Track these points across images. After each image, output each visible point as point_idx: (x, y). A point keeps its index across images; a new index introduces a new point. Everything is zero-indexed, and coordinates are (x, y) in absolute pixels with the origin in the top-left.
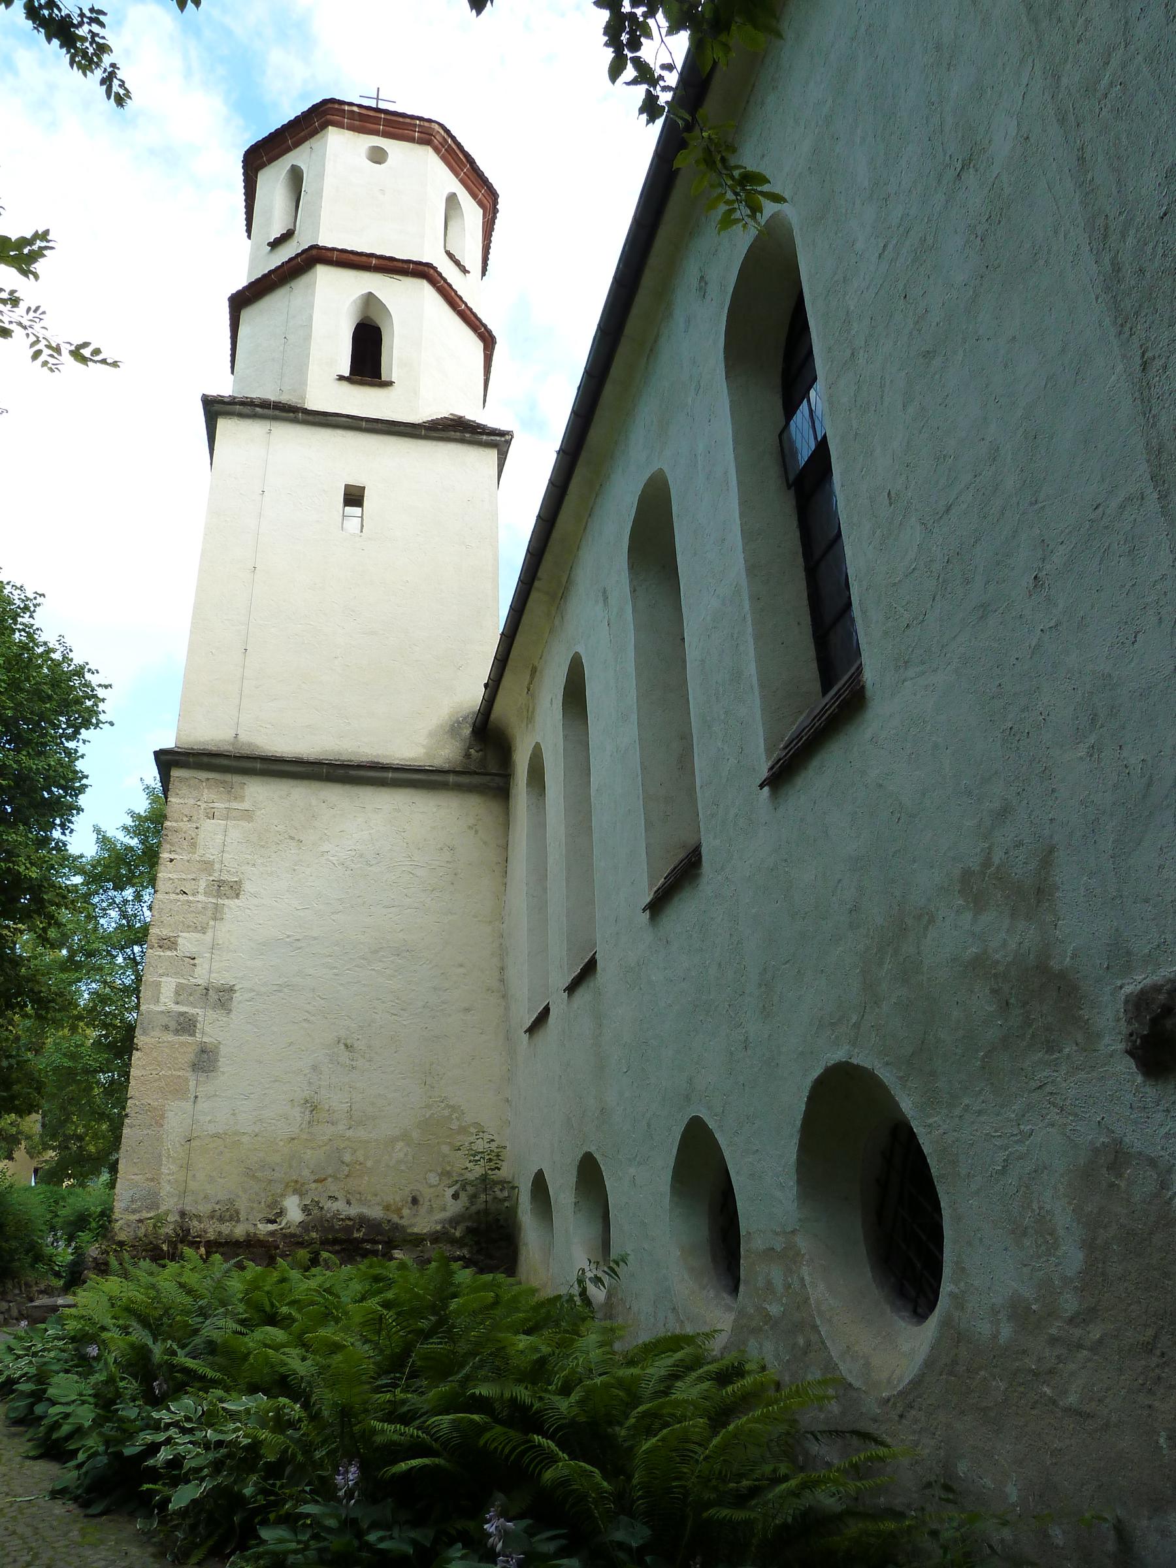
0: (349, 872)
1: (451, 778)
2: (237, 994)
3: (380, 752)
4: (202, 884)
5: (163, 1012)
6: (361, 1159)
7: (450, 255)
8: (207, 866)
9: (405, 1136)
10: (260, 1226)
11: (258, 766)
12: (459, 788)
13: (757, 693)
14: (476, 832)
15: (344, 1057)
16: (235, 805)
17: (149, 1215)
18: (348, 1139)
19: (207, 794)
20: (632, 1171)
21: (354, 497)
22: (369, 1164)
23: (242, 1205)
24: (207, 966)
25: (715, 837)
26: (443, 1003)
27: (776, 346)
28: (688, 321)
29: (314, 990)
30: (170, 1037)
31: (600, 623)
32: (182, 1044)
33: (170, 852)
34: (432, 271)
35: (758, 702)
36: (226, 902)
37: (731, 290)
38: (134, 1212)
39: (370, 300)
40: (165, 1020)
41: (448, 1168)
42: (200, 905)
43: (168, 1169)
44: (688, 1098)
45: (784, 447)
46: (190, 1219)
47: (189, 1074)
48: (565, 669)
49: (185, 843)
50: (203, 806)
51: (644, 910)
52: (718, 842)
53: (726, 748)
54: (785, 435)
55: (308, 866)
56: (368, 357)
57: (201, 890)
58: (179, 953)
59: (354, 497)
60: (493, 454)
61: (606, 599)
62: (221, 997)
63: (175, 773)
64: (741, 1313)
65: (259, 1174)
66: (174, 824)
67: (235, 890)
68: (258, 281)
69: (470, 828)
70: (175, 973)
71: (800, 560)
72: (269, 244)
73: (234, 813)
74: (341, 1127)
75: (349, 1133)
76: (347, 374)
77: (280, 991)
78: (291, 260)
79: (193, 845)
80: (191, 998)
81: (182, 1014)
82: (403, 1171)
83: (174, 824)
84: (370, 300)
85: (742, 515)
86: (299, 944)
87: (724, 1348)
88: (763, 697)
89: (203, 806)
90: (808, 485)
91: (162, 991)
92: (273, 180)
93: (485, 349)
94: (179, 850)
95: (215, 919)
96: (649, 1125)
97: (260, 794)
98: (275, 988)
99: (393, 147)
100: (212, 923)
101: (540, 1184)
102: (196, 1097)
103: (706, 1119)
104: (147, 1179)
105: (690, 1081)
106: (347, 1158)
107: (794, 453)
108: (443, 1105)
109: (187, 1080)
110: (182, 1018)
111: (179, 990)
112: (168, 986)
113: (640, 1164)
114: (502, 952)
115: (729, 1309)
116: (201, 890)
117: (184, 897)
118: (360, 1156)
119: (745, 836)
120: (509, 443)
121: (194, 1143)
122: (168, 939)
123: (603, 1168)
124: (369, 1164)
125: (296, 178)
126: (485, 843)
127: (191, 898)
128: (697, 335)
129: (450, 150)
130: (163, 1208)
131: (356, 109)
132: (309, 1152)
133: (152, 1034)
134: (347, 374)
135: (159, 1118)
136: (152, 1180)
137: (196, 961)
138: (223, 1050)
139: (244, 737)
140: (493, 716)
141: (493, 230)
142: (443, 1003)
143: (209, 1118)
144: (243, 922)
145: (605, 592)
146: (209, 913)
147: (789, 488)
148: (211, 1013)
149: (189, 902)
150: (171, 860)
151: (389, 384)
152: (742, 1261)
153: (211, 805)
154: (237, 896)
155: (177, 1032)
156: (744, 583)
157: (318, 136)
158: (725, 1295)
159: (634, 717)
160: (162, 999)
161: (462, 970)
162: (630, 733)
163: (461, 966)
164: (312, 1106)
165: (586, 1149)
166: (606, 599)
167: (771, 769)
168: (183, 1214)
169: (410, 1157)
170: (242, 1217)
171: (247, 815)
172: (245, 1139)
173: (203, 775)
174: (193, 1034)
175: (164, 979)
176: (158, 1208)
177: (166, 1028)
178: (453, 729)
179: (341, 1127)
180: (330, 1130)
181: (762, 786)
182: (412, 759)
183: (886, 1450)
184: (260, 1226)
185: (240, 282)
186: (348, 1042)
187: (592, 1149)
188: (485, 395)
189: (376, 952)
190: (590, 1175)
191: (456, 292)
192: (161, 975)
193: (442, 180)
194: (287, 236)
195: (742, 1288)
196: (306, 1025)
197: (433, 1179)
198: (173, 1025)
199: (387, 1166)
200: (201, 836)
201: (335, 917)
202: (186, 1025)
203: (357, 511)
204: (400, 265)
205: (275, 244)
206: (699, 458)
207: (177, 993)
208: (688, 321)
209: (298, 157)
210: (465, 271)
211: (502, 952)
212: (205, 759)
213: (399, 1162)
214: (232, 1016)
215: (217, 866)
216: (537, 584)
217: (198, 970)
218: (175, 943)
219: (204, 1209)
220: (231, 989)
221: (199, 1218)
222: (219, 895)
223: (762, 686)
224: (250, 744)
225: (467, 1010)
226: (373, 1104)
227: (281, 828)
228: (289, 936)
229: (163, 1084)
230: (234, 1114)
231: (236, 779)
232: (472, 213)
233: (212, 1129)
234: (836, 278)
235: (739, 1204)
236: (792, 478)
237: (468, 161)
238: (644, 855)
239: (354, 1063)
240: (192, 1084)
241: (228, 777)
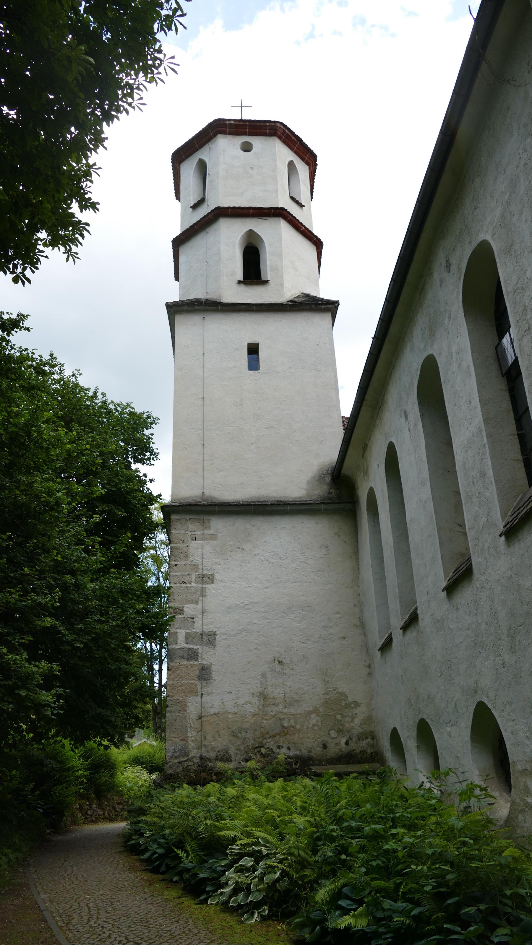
0: (271, 564)
1: (322, 507)
2: (218, 637)
3: (281, 495)
4: (193, 577)
5: (180, 649)
6: (293, 724)
7: (292, 198)
8: (195, 567)
9: (316, 711)
10: (242, 763)
11: (217, 509)
12: (327, 512)
13: (494, 486)
14: (339, 536)
15: (278, 668)
16: (206, 532)
17: (184, 759)
18: (285, 714)
19: (191, 526)
20: (449, 729)
21: (253, 350)
22: (298, 727)
23: (232, 752)
24: (200, 622)
25: (478, 557)
26: (330, 635)
27: (488, 306)
28: (441, 281)
29: (258, 632)
30: (185, 662)
31: (403, 427)
32: (192, 666)
33: (175, 561)
34: (284, 212)
35: (495, 490)
36: (207, 586)
37: (464, 271)
38: (176, 758)
39: (251, 234)
40: (181, 653)
41: (341, 728)
42: (193, 589)
43: (191, 734)
44: (476, 691)
45: (499, 353)
46: (206, 761)
47: (198, 683)
48: (385, 449)
49: (182, 555)
50: (190, 534)
51: (443, 590)
52: (480, 559)
53: (480, 511)
54: (499, 347)
55: (249, 563)
56: (253, 269)
57: (193, 580)
58: (185, 616)
59: (253, 350)
60: (329, 316)
61: (406, 416)
62: (209, 639)
63: (173, 517)
64: (513, 803)
65: (239, 735)
66: (175, 545)
67: (211, 579)
68: (187, 230)
69: (335, 534)
70: (185, 627)
71: (512, 414)
72: (191, 207)
73: (206, 536)
74: (281, 707)
75: (285, 710)
76: (242, 280)
77: (241, 634)
78: (205, 216)
79: (187, 556)
80: (194, 640)
81: (190, 649)
82: (316, 730)
83: (175, 545)
84: (251, 234)
85: (479, 392)
86: (247, 607)
87: (507, 820)
88: (498, 489)
89: (190, 534)
90: (512, 376)
91: (179, 637)
92: (189, 169)
93: (317, 249)
94: (179, 559)
95: (202, 596)
96: (456, 705)
97: (219, 525)
98: (238, 632)
99: (257, 142)
100: (201, 598)
101: (395, 736)
102: (202, 694)
103: (486, 702)
104: (181, 740)
105: (476, 682)
106: (286, 724)
107: (505, 359)
108: (335, 692)
109: (196, 685)
110: (190, 651)
111: (188, 637)
112: (181, 634)
113: (452, 725)
114: (360, 604)
115: (507, 801)
116: (193, 580)
117: (184, 585)
118: (292, 722)
119: (495, 562)
120: (337, 307)
121: (203, 719)
122: (179, 608)
123: (432, 727)
124: (298, 727)
125: (202, 167)
126: (345, 542)
127: (188, 585)
128: (447, 291)
129: (287, 136)
130: (191, 756)
131: (232, 122)
132: (265, 722)
133: (176, 661)
134: (242, 280)
135: (184, 706)
136: (184, 740)
137: (194, 620)
138: (214, 668)
139: (208, 493)
140: (343, 471)
141: (315, 175)
142: (330, 635)
143: (210, 705)
144: (217, 596)
145: (405, 412)
146: (199, 593)
147: (503, 376)
148: (205, 648)
149: (188, 587)
150: (176, 565)
151: (266, 282)
152: (511, 776)
153: (194, 533)
154: (213, 582)
155: (188, 659)
156: (483, 427)
157: (213, 140)
158: (505, 794)
159: (428, 485)
160: (179, 642)
161: (339, 616)
162: (426, 492)
163: (338, 613)
164: (264, 696)
165: (420, 717)
166: (406, 416)
167: (505, 526)
168: (201, 758)
169: (320, 723)
170: (233, 758)
171: (213, 537)
172: (230, 716)
173: (188, 517)
174: (197, 660)
175: (178, 631)
176: (188, 756)
177: (182, 657)
178: (320, 478)
179: (281, 707)
180: (275, 709)
181: (501, 535)
182: (299, 498)
183: (495, 800)
184: (242, 763)
185: (177, 232)
186: (280, 659)
187: (425, 717)
188: (319, 271)
189: (290, 608)
190: (424, 733)
191: (298, 221)
192: (177, 629)
193: (284, 154)
194: (201, 202)
195: (513, 789)
196: (255, 651)
197: (333, 734)
198: (186, 655)
199: (308, 728)
200: (190, 551)
201: (266, 590)
202: (193, 655)
203: (255, 356)
204: (266, 211)
205: (195, 207)
206: (453, 355)
207: (186, 638)
208: (441, 281)
209: (203, 154)
210: (301, 206)
211: (360, 604)
212: (188, 508)
213: (314, 725)
214: (216, 648)
215: (200, 567)
216: (365, 402)
217: (196, 625)
218: (182, 611)
219: (212, 755)
220: (215, 634)
221: (210, 760)
222: (203, 582)
223: (496, 482)
224: (211, 497)
225: (344, 638)
226: (296, 693)
227: (232, 543)
228: (242, 603)
229: (184, 688)
230: (222, 703)
231: (206, 517)
232: (302, 169)
233: (212, 711)
234: (518, 286)
235: (507, 747)
236: (504, 372)
237: (297, 140)
238: (440, 560)
239: (284, 671)
240: (199, 687)
241: (201, 517)
